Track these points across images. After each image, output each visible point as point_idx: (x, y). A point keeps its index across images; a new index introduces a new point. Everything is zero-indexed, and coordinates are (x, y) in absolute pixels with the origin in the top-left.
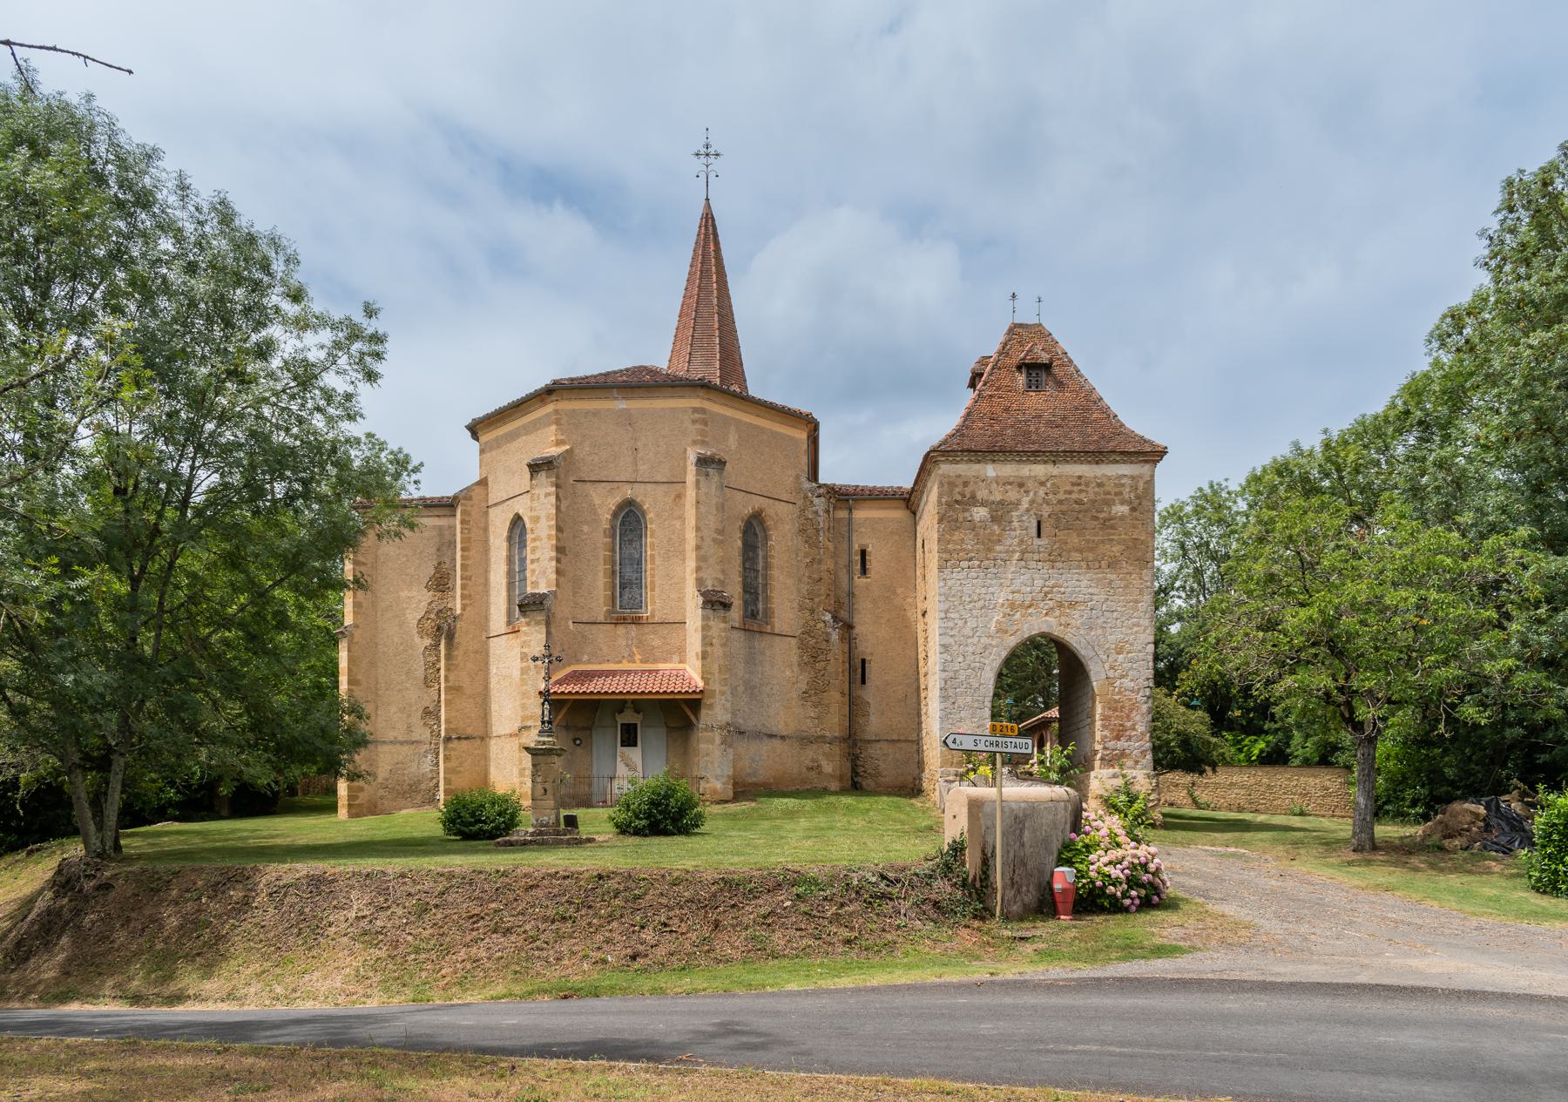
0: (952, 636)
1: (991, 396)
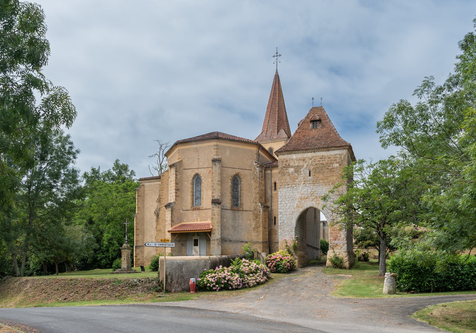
1: (300, 132)
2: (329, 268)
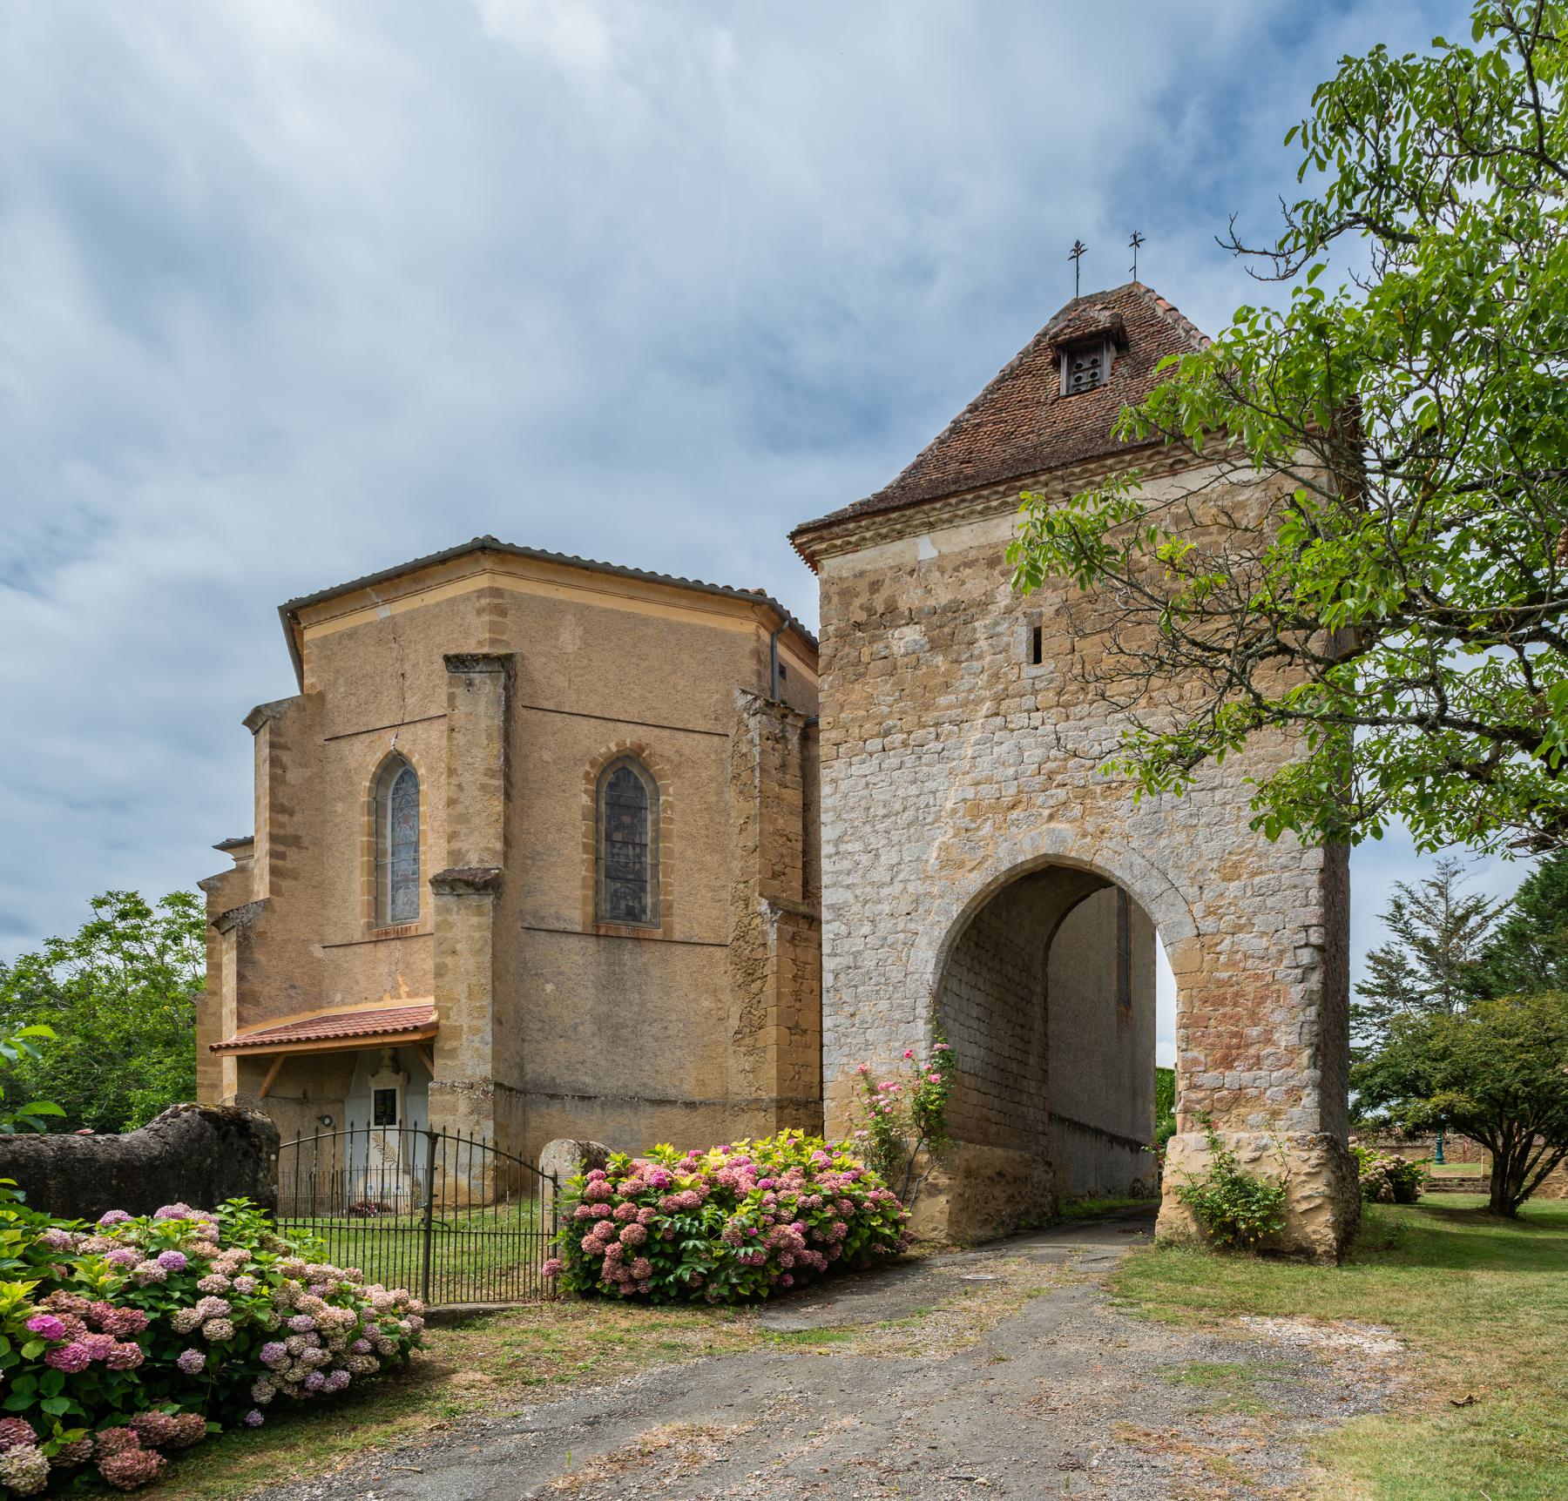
0: (848, 887)
2: (1174, 1255)
